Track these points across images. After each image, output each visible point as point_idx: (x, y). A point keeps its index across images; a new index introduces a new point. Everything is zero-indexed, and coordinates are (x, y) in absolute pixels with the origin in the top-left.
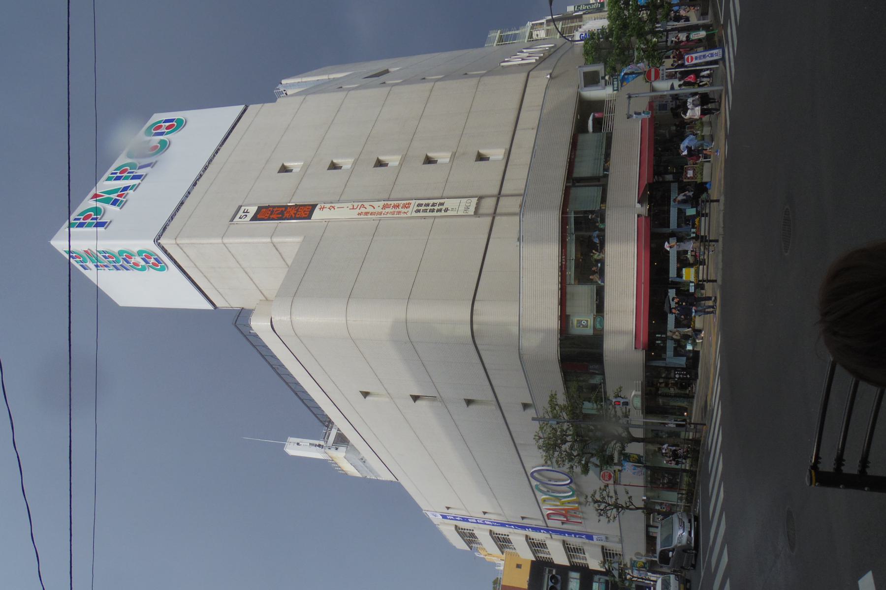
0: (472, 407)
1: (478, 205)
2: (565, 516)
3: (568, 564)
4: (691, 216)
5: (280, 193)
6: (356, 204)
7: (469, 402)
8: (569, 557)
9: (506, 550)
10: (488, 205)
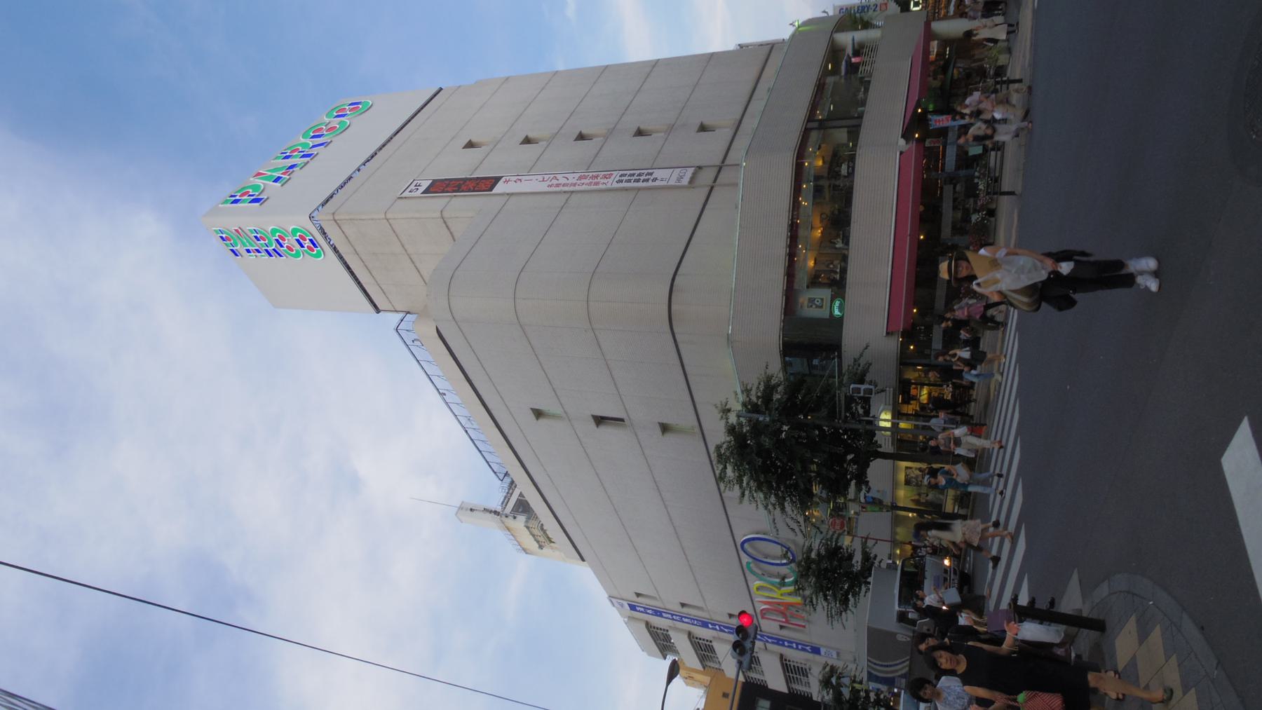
0: (669, 437)
1: (694, 174)
2: (784, 615)
3: (785, 690)
4: (975, 156)
5: (460, 166)
6: (546, 177)
7: (665, 428)
8: (788, 680)
9: (709, 664)
10: (707, 177)
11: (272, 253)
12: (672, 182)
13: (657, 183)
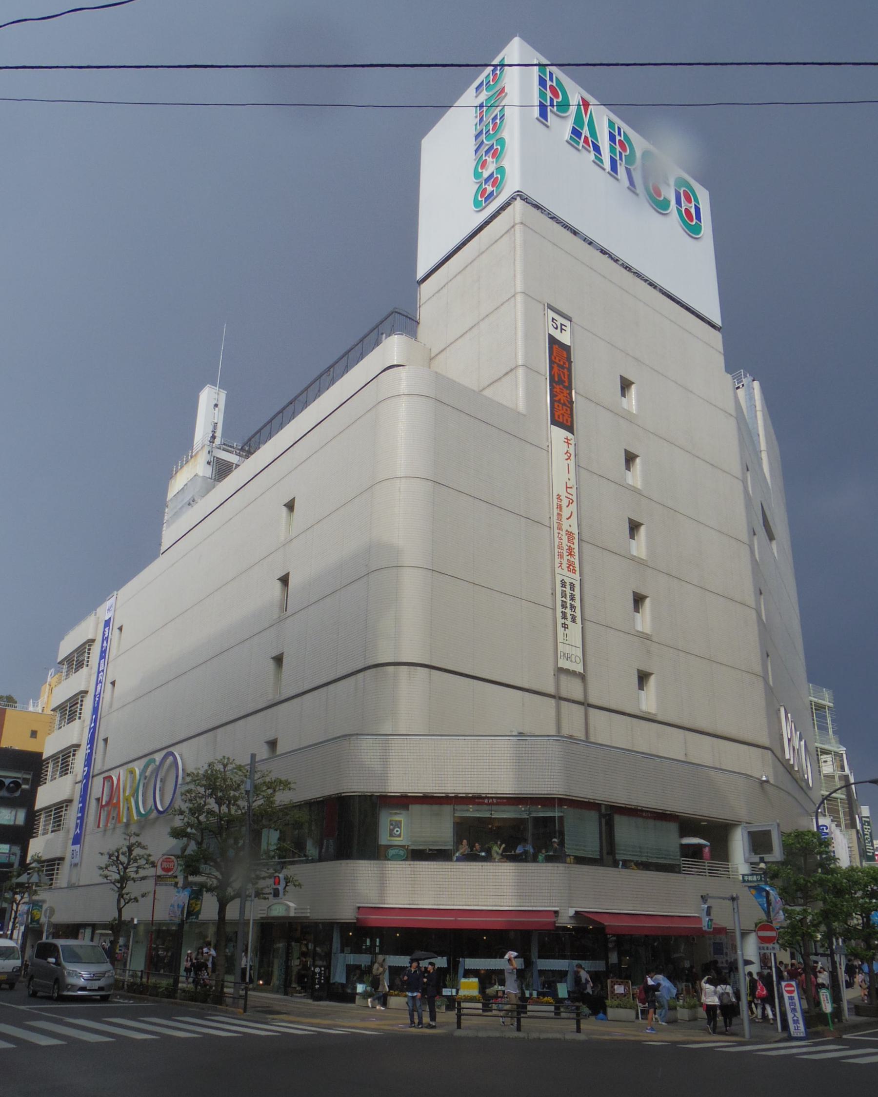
2: (108, 803)
3: (37, 807)
4: (556, 990)
5: (590, 378)
6: (573, 491)
7: (278, 660)
8: (47, 809)
10: (573, 688)
11: (480, 140)
12: (560, 647)
13: (560, 630)
